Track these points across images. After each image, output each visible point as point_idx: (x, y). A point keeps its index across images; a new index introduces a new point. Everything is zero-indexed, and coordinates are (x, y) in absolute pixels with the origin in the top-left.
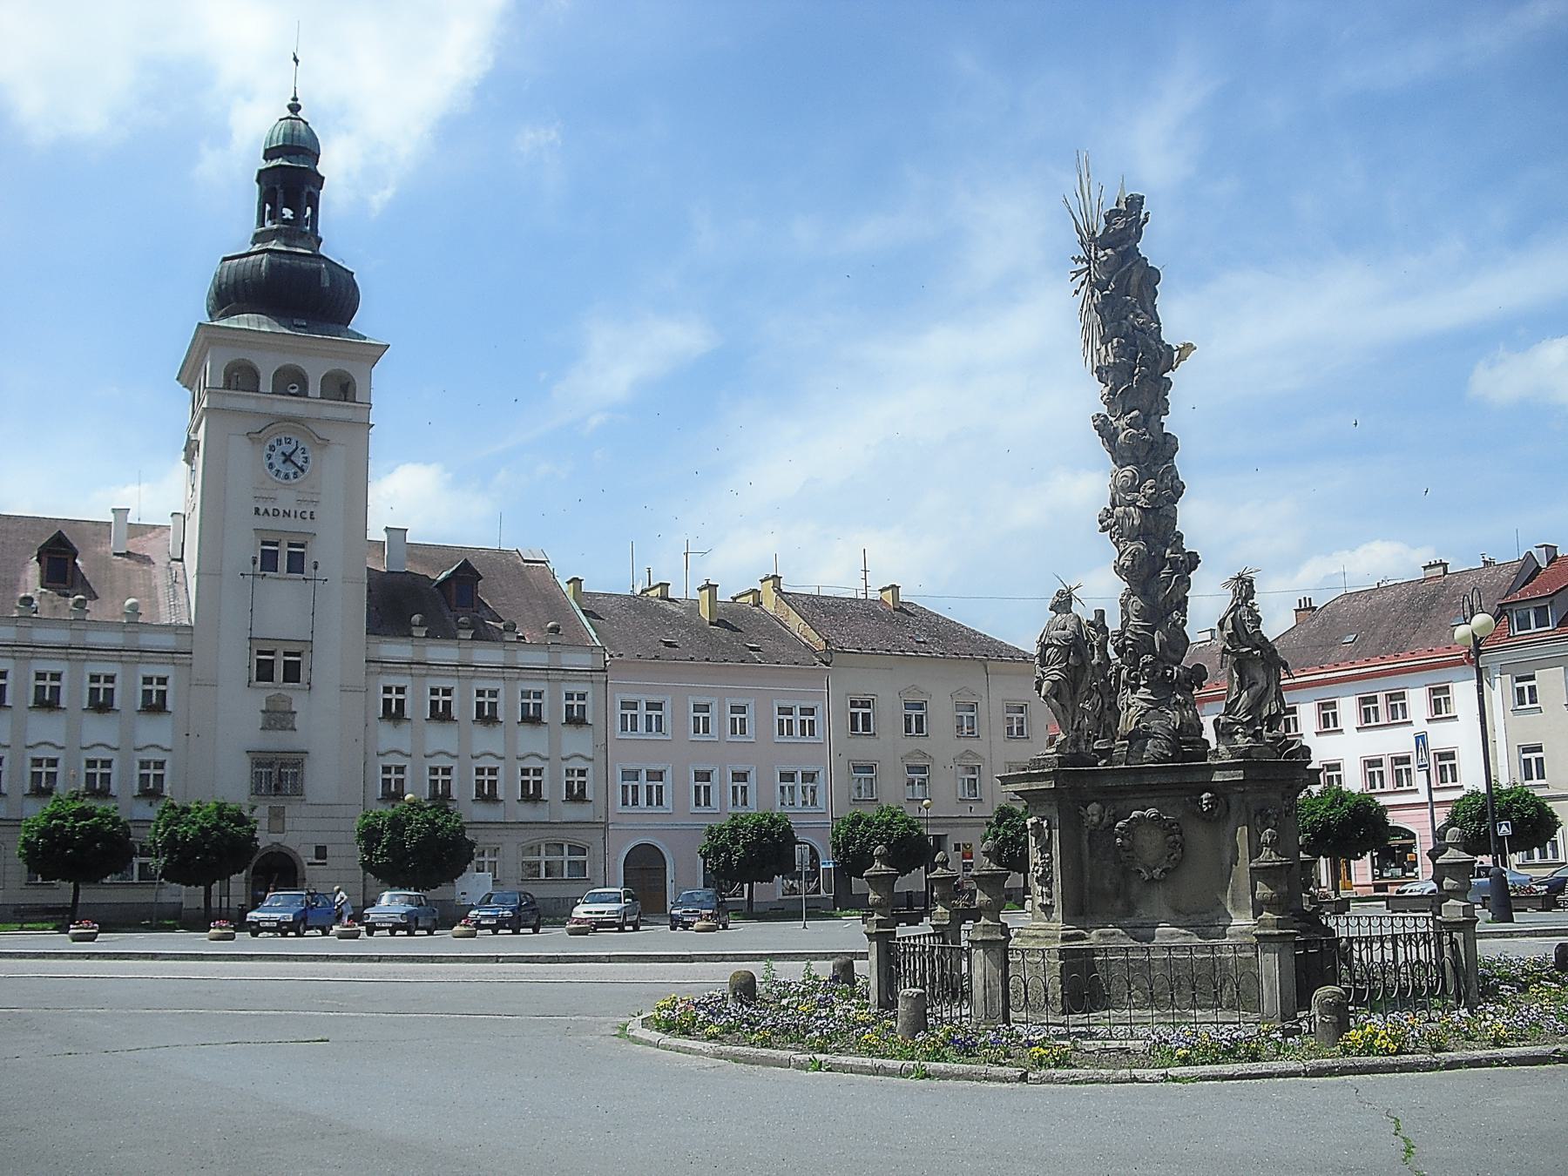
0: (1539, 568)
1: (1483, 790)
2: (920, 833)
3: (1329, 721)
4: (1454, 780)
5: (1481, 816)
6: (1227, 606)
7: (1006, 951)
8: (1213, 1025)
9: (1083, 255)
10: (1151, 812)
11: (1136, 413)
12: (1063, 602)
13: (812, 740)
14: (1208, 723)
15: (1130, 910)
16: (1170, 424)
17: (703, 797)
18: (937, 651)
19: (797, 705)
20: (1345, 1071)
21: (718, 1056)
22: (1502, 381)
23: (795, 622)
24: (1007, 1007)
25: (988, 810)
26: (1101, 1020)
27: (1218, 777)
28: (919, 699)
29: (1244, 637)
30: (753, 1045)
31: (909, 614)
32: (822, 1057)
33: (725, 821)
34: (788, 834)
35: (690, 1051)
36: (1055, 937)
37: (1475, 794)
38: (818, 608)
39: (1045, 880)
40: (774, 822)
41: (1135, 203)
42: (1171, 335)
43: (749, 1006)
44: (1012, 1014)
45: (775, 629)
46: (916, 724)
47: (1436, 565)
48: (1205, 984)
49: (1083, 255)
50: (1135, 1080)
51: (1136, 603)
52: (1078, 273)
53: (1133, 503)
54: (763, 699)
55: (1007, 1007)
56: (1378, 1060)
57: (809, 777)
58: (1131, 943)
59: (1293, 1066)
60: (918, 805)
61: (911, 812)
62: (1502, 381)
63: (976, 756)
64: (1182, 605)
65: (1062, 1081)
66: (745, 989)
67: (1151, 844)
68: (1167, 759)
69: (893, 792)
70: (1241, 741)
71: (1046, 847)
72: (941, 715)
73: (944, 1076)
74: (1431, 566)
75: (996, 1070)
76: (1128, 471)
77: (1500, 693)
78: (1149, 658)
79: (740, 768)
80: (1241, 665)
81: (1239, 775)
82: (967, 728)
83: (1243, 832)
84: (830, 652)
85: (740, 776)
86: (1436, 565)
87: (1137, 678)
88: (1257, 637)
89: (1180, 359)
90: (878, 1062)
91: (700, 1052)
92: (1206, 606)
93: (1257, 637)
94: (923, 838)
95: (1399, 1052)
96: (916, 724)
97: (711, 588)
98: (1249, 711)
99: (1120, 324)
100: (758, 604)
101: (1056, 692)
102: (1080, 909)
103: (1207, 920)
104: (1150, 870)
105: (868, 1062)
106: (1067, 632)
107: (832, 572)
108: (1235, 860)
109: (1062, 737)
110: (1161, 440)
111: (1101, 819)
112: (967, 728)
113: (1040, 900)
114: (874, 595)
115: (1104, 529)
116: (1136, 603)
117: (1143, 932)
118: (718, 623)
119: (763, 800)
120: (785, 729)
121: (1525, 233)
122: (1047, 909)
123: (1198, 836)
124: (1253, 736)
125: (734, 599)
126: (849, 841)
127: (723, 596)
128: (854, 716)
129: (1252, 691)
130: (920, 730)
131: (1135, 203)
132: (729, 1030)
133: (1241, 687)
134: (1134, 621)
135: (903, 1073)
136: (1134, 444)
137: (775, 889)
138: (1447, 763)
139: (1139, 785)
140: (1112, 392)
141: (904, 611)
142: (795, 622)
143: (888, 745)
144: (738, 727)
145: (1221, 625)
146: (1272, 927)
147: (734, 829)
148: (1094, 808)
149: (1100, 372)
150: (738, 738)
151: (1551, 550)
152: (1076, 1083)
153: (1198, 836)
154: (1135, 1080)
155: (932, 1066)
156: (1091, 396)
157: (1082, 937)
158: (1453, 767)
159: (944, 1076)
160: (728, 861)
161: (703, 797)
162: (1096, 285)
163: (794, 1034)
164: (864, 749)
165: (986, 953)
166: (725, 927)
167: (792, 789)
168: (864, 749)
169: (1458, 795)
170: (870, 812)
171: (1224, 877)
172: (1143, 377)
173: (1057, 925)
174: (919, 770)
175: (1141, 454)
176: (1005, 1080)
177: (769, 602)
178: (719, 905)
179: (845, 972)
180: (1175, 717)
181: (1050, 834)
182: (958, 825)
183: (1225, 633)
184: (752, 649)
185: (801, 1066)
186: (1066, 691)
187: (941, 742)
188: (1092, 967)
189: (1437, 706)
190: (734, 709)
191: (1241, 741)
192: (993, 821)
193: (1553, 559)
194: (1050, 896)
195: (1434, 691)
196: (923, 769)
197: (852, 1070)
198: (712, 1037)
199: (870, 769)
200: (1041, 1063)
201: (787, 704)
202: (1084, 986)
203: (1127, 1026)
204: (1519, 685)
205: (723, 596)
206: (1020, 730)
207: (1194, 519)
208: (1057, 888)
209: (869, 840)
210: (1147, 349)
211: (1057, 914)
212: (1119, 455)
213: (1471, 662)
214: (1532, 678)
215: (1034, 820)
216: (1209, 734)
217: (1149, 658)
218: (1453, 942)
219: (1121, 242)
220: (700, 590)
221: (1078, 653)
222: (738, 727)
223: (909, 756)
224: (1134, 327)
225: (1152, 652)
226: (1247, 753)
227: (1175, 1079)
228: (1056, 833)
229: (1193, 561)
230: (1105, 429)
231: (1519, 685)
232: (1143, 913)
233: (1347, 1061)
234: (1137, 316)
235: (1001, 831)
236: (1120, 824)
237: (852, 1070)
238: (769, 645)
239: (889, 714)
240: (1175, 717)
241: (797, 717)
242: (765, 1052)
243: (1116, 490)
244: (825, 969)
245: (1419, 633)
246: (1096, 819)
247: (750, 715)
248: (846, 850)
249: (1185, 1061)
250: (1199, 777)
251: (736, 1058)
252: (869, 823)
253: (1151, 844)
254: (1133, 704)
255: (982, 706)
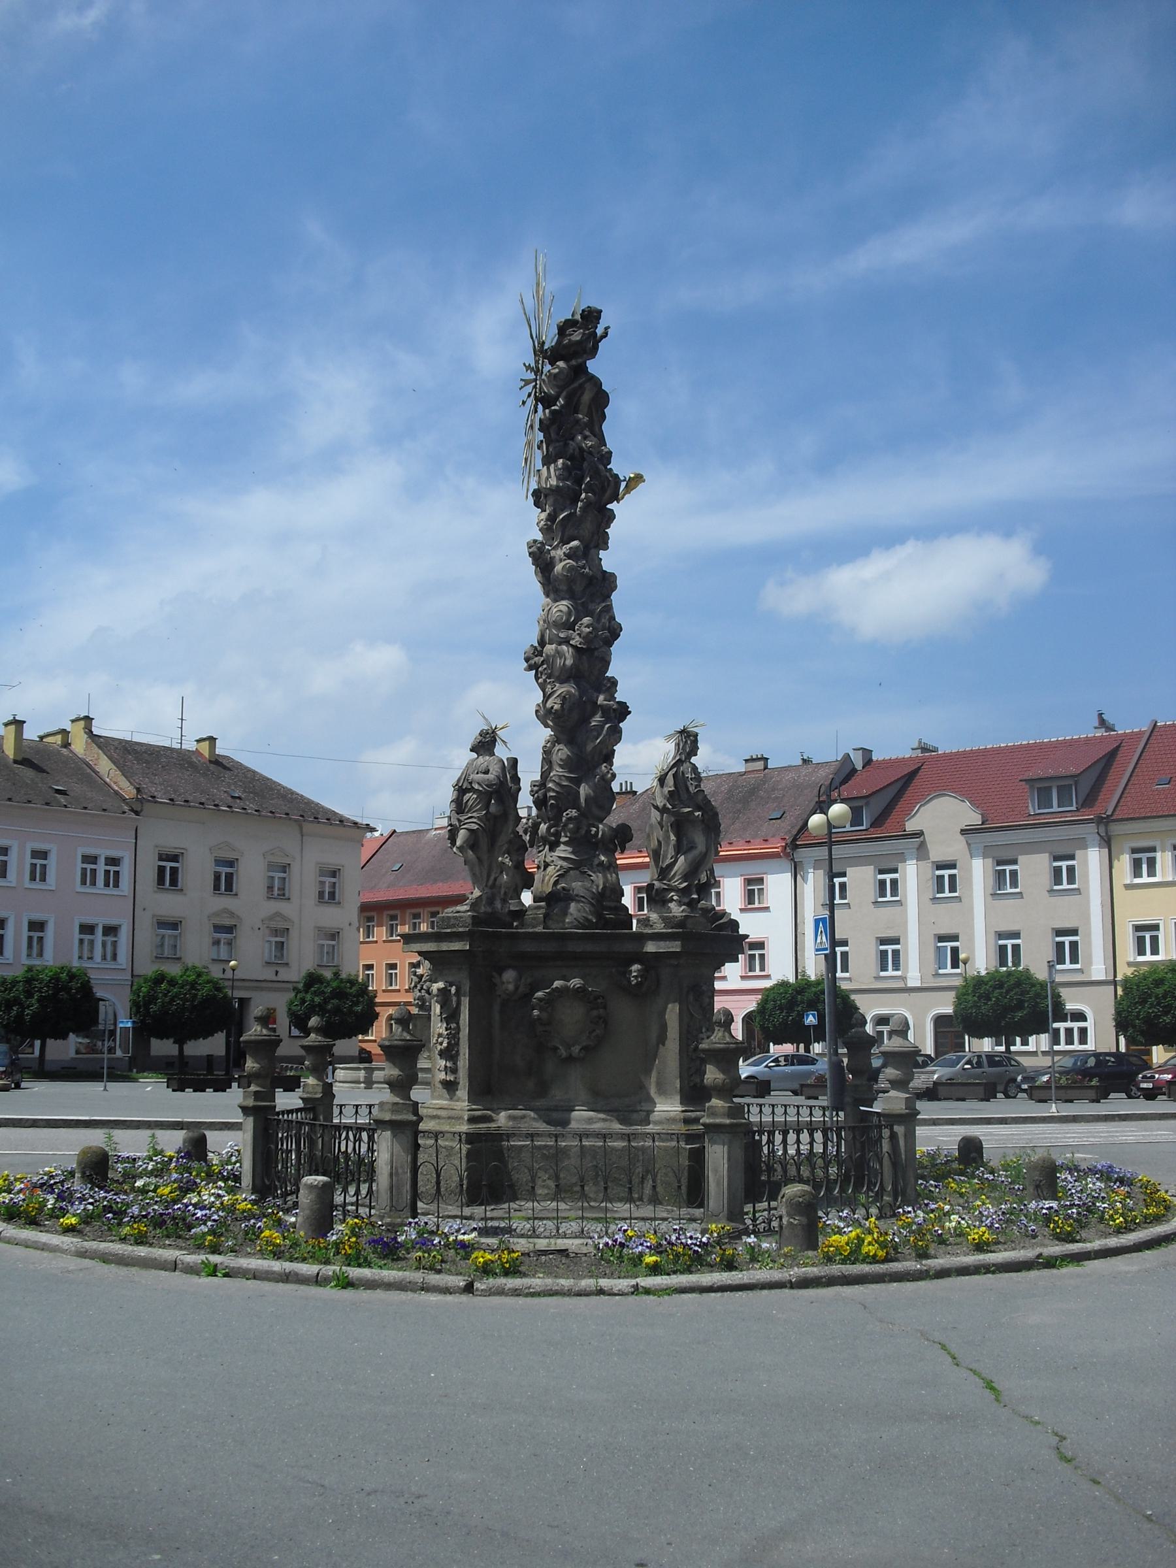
0: (854, 771)
1: (792, 980)
2: (225, 996)
3: (753, 893)
4: (762, 969)
5: (791, 1004)
6: (670, 760)
7: (416, 1133)
8: (639, 1225)
9: (533, 365)
10: (576, 982)
11: (575, 543)
12: (486, 743)
13: (115, 892)
14: (628, 890)
15: (543, 1089)
16: (608, 560)
17: (36, 944)
18: (251, 807)
19: (103, 853)
20: (831, 1281)
21: (82, 1254)
22: (794, 598)
23: (104, 766)
24: (415, 1196)
25: (295, 973)
26: (517, 1214)
27: (651, 947)
28: (231, 856)
29: (684, 796)
30: (123, 1240)
31: (225, 768)
32: (215, 1259)
33: (18, 972)
34: (86, 989)
35: (43, 1247)
36: (460, 1118)
37: (784, 984)
38: (127, 753)
39: (449, 1053)
40: (72, 976)
41: (591, 316)
42: (620, 467)
43: (101, 1188)
44: (420, 1204)
45: (84, 772)
46: (224, 883)
47: (758, 759)
48: (612, 1178)
49: (533, 365)
50: (601, 1292)
51: (562, 752)
52: (527, 382)
53: (566, 641)
54: (67, 846)
55: (415, 1196)
56: (866, 1268)
57: (111, 930)
58: (542, 1127)
59: (776, 1275)
60: (222, 966)
61: (216, 972)
62: (794, 598)
63: (285, 919)
64: (609, 757)
65: (516, 1292)
66: (97, 1167)
67: (571, 1016)
68: (590, 925)
69: (196, 950)
70: (677, 910)
71: (451, 1016)
72: (252, 874)
73: (371, 1285)
74: (752, 760)
75: (434, 1279)
76: (564, 605)
77: (1124, 863)
78: (573, 813)
79: (37, 916)
80: (680, 826)
81: (675, 947)
82: (278, 891)
83: (672, 1013)
84: (141, 801)
85: (37, 926)
86: (758, 759)
87: (557, 835)
88: (700, 797)
89: (628, 489)
90: (288, 1266)
91: (54, 1249)
92: (639, 760)
93: (700, 797)
94: (227, 1001)
95: (886, 1260)
96: (224, 883)
97: (18, 724)
98: (685, 877)
99: (566, 445)
100: (66, 745)
101: (473, 843)
102: (487, 1088)
103: (629, 1105)
104: (568, 1046)
105: (277, 1266)
106: (491, 776)
107: (152, 714)
108: (662, 1039)
109: (477, 893)
110: (599, 576)
111: (517, 988)
112: (278, 891)
113: (442, 1076)
114: (190, 745)
115: (530, 668)
116: (562, 752)
117: (558, 1116)
118: (25, 762)
119: (59, 952)
120: (87, 878)
121: (831, 462)
122: (450, 1087)
123: (623, 1010)
124: (688, 904)
125: (41, 738)
126: (151, 999)
127: (31, 733)
128: (161, 870)
129: (691, 855)
130: (229, 887)
131: (591, 316)
132: (87, 1219)
133: (679, 850)
134: (557, 771)
135: (318, 1281)
136: (572, 576)
137: (67, 1048)
138: (757, 952)
139: (558, 952)
140: (552, 518)
141: (220, 764)
142: (104, 766)
143: (195, 902)
144: (38, 874)
145: (662, 780)
146: (723, 1115)
147: (28, 981)
148: (509, 975)
149: (539, 497)
150: (37, 885)
151: (867, 752)
152: (533, 1295)
153: (623, 1010)
154: (601, 1292)
155: (355, 1272)
156: (529, 523)
157: (489, 1119)
158: (762, 956)
159: (371, 1285)
160: (20, 1016)
161: (36, 944)
162: (545, 400)
163: (172, 1225)
164: (169, 904)
165: (394, 1136)
166: (18, 1086)
167: (92, 942)
168: (169, 904)
169: (767, 984)
170: (174, 970)
171: (648, 1058)
172: (588, 505)
173: (462, 1103)
174: (226, 930)
175: (578, 588)
176: (446, 1291)
177: (79, 744)
178: (13, 1063)
179: (197, 1148)
180: (598, 879)
181: (459, 1003)
182: (262, 989)
183: (666, 790)
184: (58, 791)
185: (191, 1270)
186: (484, 842)
187: (251, 903)
188: (499, 1155)
189: (750, 896)
190: (36, 854)
191: (677, 910)
192: (301, 986)
193: (868, 762)
194: (454, 1071)
195: (749, 882)
196: (230, 929)
197: (255, 1275)
198: (69, 1230)
199: (174, 925)
200: (486, 1270)
201: (91, 851)
202: (490, 1177)
203: (542, 1223)
204: (939, 873)
205: (31, 733)
206: (332, 895)
207: (627, 670)
208: (463, 1062)
209: (172, 1000)
210: (596, 474)
211: (463, 1093)
212: (551, 585)
213: (787, 855)
214: (1015, 862)
215: (441, 985)
216: (628, 900)
217: (573, 813)
218: (893, 1137)
219: (575, 355)
220: (6, 725)
221: (500, 801)
222: (38, 874)
223: (216, 914)
224: (581, 449)
225: (575, 804)
226: (682, 923)
227: (648, 1291)
228: (465, 1001)
229: (623, 711)
230: (541, 559)
231: (939, 873)
232: (557, 1095)
233: (836, 1269)
234: (585, 438)
235: (308, 997)
236: (539, 994)
237: (255, 1275)
238: (76, 788)
239: (198, 870)
240: (598, 879)
241: (101, 867)
242: (142, 1251)
243: (547, 623)
244: (172, 1142)
245: (737, 825)
246: (511, 987)
247: (52, 863)
248: (147, 1009)
249: (655, 1270)
250: (629, 947)
251: (105, 1258)
252: (172, 982)
253: (571, 1016)
254: (548, 864)
255: (295, 868)
